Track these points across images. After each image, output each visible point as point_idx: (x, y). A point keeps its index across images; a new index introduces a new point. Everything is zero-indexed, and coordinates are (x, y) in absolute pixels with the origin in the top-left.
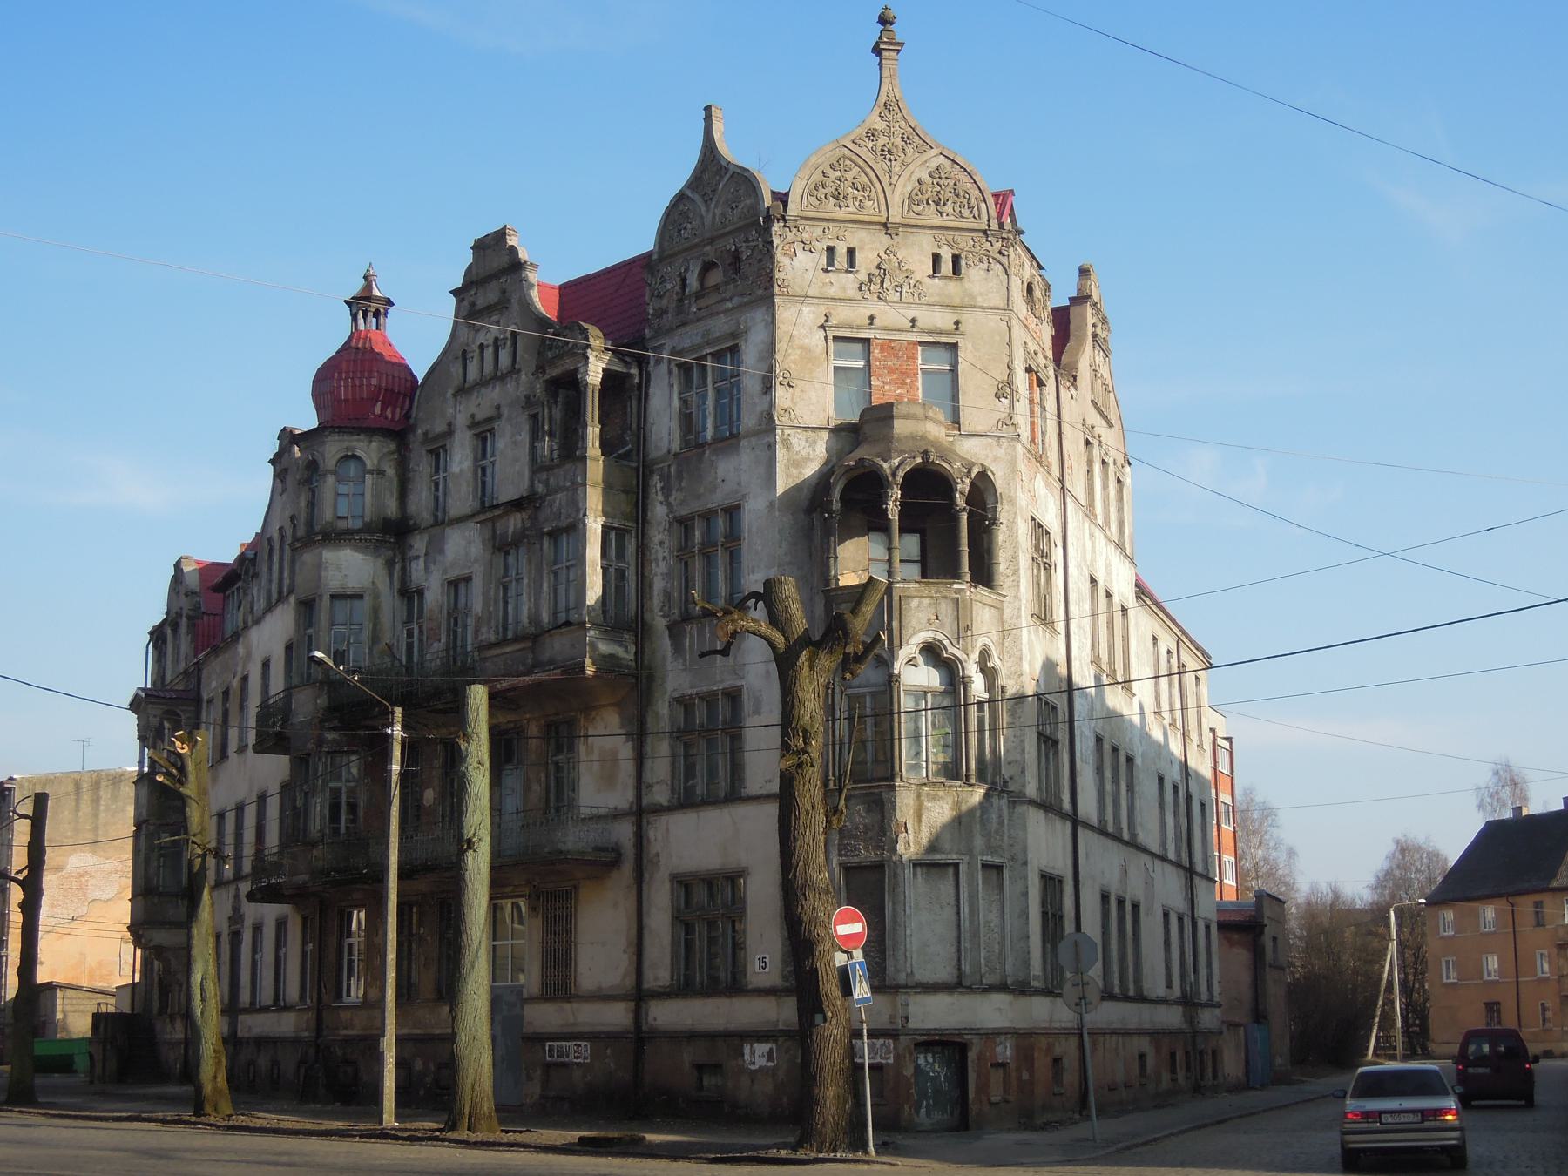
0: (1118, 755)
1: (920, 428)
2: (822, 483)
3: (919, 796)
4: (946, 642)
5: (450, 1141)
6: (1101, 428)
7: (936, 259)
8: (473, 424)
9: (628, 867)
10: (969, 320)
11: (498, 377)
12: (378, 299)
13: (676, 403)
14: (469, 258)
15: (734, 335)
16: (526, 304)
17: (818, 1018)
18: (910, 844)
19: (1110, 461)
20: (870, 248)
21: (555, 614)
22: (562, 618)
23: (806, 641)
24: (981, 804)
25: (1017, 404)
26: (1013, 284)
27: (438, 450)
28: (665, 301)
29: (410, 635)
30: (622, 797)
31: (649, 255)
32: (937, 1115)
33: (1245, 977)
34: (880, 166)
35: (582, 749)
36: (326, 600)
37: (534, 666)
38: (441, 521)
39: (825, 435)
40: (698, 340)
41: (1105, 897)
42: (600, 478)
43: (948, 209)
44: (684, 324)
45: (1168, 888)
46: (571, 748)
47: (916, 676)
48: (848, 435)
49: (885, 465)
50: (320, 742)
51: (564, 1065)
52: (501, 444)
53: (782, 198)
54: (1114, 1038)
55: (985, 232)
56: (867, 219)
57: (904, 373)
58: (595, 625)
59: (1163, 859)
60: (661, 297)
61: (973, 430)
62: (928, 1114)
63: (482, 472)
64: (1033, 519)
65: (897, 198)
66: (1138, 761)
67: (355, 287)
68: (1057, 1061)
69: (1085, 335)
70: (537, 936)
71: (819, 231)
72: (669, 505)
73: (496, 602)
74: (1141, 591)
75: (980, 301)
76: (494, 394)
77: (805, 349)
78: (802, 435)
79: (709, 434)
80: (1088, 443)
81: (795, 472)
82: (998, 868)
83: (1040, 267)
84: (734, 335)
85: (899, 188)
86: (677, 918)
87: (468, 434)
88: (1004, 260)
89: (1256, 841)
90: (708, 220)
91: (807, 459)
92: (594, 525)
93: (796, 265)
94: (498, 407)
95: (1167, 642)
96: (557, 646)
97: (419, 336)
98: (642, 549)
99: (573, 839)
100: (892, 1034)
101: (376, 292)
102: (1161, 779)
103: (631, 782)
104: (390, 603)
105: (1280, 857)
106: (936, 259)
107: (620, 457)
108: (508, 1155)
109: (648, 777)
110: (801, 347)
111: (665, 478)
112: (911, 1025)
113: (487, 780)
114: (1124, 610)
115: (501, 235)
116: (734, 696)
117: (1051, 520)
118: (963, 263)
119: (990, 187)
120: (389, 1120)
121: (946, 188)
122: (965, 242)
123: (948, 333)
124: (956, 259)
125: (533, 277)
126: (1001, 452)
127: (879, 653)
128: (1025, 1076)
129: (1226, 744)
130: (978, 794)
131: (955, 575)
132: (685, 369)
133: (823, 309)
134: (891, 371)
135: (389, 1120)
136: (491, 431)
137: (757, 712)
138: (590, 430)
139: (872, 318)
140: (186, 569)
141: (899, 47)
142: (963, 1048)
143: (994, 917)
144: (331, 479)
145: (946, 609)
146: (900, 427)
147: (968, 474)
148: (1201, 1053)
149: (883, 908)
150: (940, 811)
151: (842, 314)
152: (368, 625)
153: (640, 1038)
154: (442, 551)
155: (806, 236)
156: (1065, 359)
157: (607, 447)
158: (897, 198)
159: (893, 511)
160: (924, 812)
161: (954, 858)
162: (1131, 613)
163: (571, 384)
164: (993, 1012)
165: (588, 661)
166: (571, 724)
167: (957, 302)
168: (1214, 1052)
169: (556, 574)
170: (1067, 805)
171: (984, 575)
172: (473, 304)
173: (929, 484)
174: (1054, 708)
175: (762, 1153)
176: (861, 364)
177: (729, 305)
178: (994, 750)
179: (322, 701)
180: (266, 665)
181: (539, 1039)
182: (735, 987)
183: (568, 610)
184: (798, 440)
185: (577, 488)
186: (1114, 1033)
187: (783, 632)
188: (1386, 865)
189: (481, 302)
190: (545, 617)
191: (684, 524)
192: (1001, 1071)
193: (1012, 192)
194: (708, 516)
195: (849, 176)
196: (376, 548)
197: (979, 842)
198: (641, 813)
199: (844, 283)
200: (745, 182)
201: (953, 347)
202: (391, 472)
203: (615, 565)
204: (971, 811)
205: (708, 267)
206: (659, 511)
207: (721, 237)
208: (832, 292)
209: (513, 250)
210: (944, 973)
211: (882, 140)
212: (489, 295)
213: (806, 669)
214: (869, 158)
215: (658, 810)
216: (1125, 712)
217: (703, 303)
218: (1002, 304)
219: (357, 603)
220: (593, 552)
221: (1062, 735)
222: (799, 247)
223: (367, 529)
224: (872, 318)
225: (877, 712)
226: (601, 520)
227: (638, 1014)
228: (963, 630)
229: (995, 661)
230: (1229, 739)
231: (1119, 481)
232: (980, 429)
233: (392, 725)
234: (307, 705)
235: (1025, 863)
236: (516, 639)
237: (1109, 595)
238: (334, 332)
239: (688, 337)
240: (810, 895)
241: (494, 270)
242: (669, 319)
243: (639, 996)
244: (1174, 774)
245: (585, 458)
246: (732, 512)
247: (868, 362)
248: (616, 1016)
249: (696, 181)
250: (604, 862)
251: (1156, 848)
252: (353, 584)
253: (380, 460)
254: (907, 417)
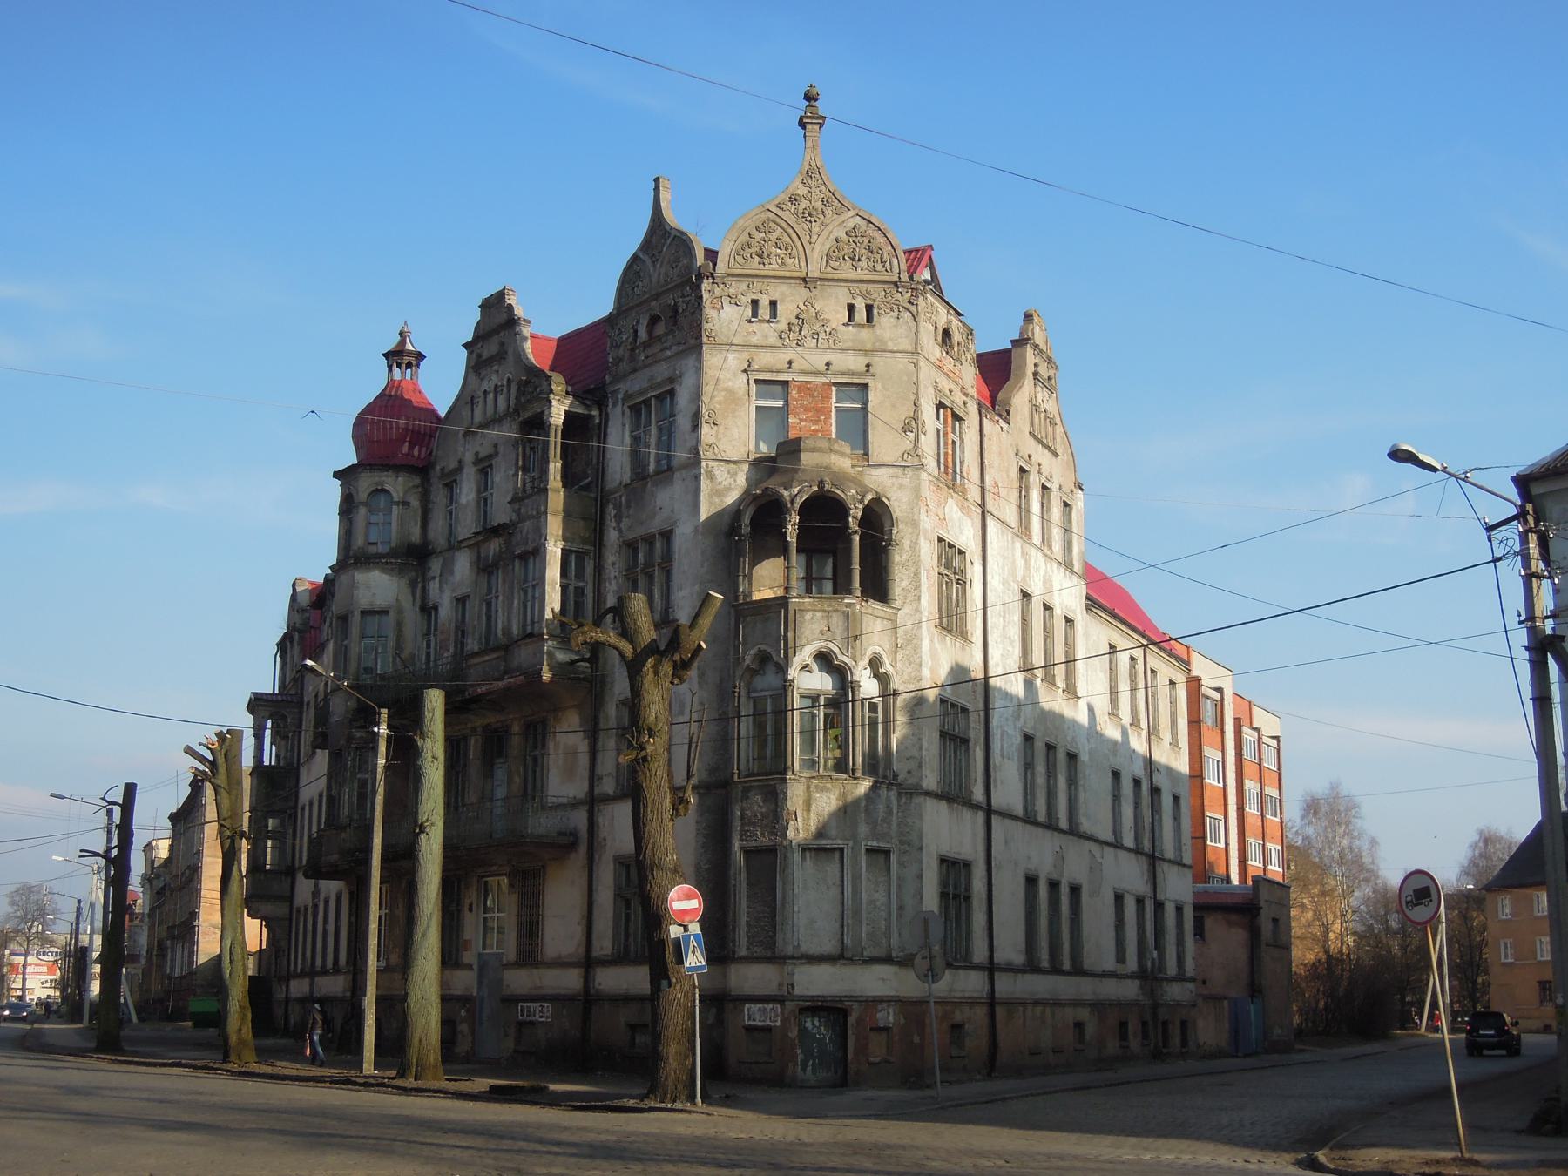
0: (1053, 753)
1: (828, 459)
2: (735, 512)
3: (808, 788)
4: (836, 650)
5: (393, 1087)
6: (1041, 455)
7: (851, 308)
9: (583, 849)
10: (879, 363)
12: (410, 352)
13: (628, 440)
14: (476, 316)
15: (671, 380)
16: (520, 356)
17: (664, 983)
18: (800, 829)
19: (1054, 487)
20: (791, 300)
21: (525, 625)
22: (529, 629)
23: (652, 649)
24: (867, 795)
25: (922, 437)
26: (921, 329)
27: (451, 485)
28: (621, 351)
29: (428, 646)
30: (578, 789)
32: (822, 1074)
33: (1242, 955)
34: (801, 228)
35: (551, 745)
36: (357, 617)
37: (505, 673)
38: (454, 546)
39: (746, 467)
40: (646, 385)
41: (1031, 881)
42: (561, 507)
43: (863, 264)
44: (635, 371)
45: (1128, 874)
46: (544, 745)
47: (810, 681)
48: (765, 467)
49: (786, 494)
50: (350, 739)
51: (532, 1023)
53: (712, 255)
54: (1039, 1009)
55: (895, 284)
56: (788, 274)
57: (819, 411)
58: (552, 636)
59: (1117, 845)
60: (618, 347)
61: (880, 461)
62: (814, 1071)
63: (483, 501)
64: (940, 540)
65: (816, 255)
66: (1084, 757)
67: (391, 343)
68: (957, 1028)
69: (1024, 374)
70: (514, 909)
71: (744, 287)
72: (620, 531)
73: (480, 617)
75: (890, 346)
77: (730, 391)
78: (724, 467)
79: (652, 468)
80: (1022, 471)
81: (717, 500)
82: (887, 853)
83: (959, 314)
84: (671, 380)
85: (818, 247)
86: (619, 895)
87: (473, 469)
88: (913, 309)
89: (1341, 831)
90: (654, 280)
91: (729, 489)
92: (554, 549)
93: (723, 317)
94: (496, 446)
96: (523, 655)
97: (440, 384)
98: (599, 569)
99: (541, 825)
100: (780, 1000)
101: (409, 347)
102: (1116, 775)
103: (586, 774)
104: (412, 618)
105: (1365, 846)
106: (851, 308)
107: (582, 488)
108: (395, 1098)
109: (600, 770)
110: (726, 390)
111: (618, 507)
112: (797, 992)
113: (441, 771)
114: (1069, 621)
115: (501, 295)
118: (875, 312)
119: (903, 244)
120: (368, 1067)
121: (862, 244)
122: (878, 293)
123: (860, 375)
124: (869, 308)
125: (526, 331)
126: (906, 481)
127: (774, 662)
128: (916, 1039)
129: (1274, 743)
130: (864, 786)
131: (848, 591)
132: (635, 410)
133: (746, 356)
134: (807, 409)
135: (368, 1067)
136: (491, 466)
138: (552, 465)
139: (790, 363)
140: (298, 589)
141: (821, 121)
142: (845, 1013)
143: (880, 897)
144: (363, 511)
145: (837, 621)
146: (807, 459)
147: (861, 501)
148: (1165, 1023)
149: (774, 888)
150: (827, 802)
151: (764, 359)
152: (392, 638)
153: (588, 1000)
154: (452, 572)
155: (732, 291)
156: (1001, 395)
157: (568, 479)
158: (816, 255)
160: (812, 802)
161: (839, 843)
162: (1079, 625)
163: (538, 424)
164: (875, 981)
165: (545, 668)
166: (544, 722)
167: (869, 346)
168: (1184, 1024)
169: (525, 592)
170: (978, 794)
171: (877, 587)
172: (479, 356)
173: (825, 510)
174: (962, 713)
175: (617, 1103)
176: (780, 403)
177: (668, 353)
178: (886, 746)
179: (352, 704)
181: (511, 1000)
183: (533, 622)
184: (721, 472)
185: (541, 515)
186: (1036, 1003)
187: (632, 642)
188: (1470, 854)
189: (485, 355)
190: (515, 630)
191: (631, 546)
192: (884, 1035)
193: (931, 247)
194: (649, 540)
195: (773, 237)
196: (400, 570)
197: (863, 830)
198: (593, 802)
199: (765, 332)
200: (682, 243)
201: (865, 387)
202: (415, 503)
203: (574, 583)
204: (857, 802)
205: (654, 320)
206: (612, 536)
207: (665, 290)
208: (755, 340)
209: (510, 307)
210: (828, 946)
211: (804, 204)
212: (490, 349)
213: (651, 675)
214: (791, 220)
215: (607, 799)
216: (1068, 712)
217: (649, 352)
218: (911, 348)
219: (384, 618)
220: (553, 572)
221: (975, 733)
222: (726, 300)
223: (394, 553)
224: (790, 363)
225: (773, 713)
226: (560, 544)
227: (587, 979)
228: (852, 637)
229: (887, 667)
230: (1276, 738)
231: (1066, 504)
232: (887, 460)
233: (378, 724)
235: (921, 849)
236: (493, 650)
237: (1047, 607)
238: (372, 381)
239: (635, 384)
240: (658, 874)
241: (497, 323)
242: (624, 366)
243: (589, 963)
244: (1139, 770)
245: (546, 490)
246: (667, 535)
247: (786, 401)
248: (571, 981)
249: (647, 245)
250: (564, 845)
251: (1106, 834)
252: (381, 601)
253: (405, 493)
254: (813, 450)
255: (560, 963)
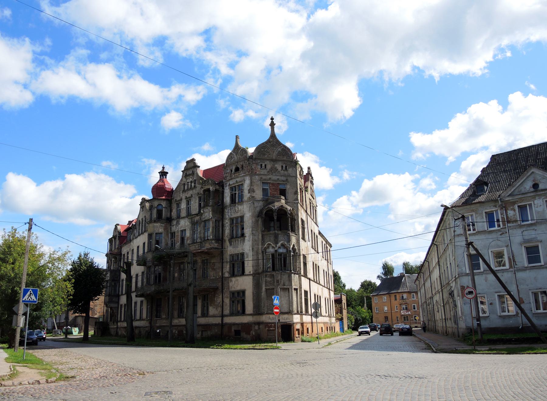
7: (282, 166)
8: (186, 198)
11: (191, 188)
27: (178, 205)
31: (224, 164)
38: (179, 217)
44: (231, 179)
52: (192, 202)
59: (324, 287)
74: (320, 233)
76: (191, 192)
87: (185, 200)
95: (324, 242)
97: (173, 181)
106: (282, 166)
116: (242, 254)
117: (305, 219)
124: (286, 167)
137: (247, 257)
151: (264, 177)
159: (275, 218)
180: (138, 247)
182: (243, 312)
189: (188, 173)
199: (264, 172)
208: (262, 173)
227: (222, 320)
234: (150, 257)
246: (242, 217)
248: (218, 320)
251: (323, 285)
255: (214, 316)
